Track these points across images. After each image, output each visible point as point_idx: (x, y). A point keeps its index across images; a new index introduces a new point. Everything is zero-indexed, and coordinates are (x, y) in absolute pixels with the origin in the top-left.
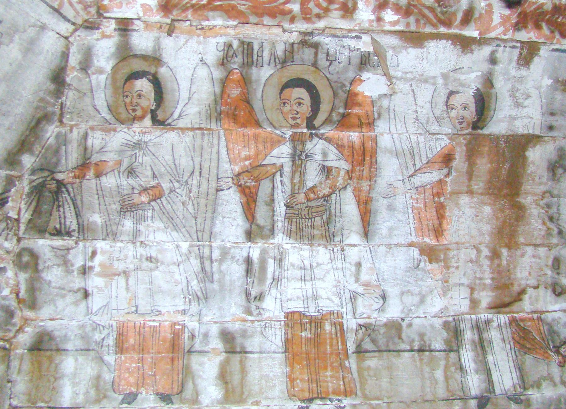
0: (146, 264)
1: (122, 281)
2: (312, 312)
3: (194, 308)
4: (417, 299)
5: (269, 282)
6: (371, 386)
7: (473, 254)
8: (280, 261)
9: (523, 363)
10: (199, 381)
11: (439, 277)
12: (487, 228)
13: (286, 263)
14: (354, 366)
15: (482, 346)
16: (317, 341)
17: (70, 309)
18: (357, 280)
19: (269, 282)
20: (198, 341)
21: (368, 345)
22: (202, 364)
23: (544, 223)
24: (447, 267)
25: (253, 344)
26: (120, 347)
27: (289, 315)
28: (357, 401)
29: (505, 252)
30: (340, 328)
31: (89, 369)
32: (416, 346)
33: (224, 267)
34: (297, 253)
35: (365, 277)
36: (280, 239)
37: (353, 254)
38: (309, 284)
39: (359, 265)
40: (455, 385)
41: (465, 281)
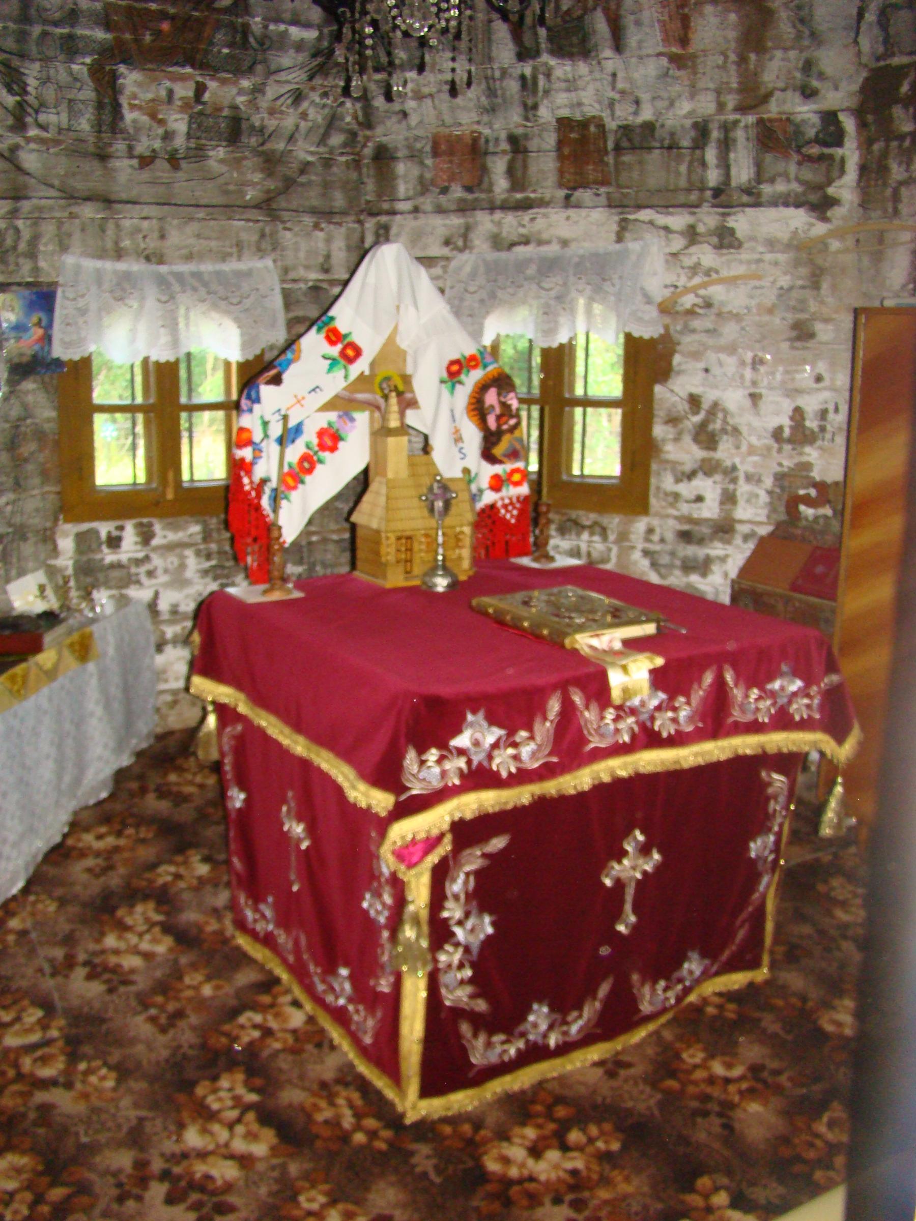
1: (429, 101)
2: (578, 117)
3: (485, 118)
4: (666, 103)
5: (540, 94)
6: (624, 177)
7: (720, 60)
8: (548, 75)
11: (687, 83)
12: (732, 35)
13: (553, 78)
15: (726, 145)
16: (584, 140)
18: (613, 88)
21: (625, 144)
23: (794, 27)
24: (695, 73)
25: (533, 145)
26: (435, 153)
27: (560, 121)
28: (610, 190)
29: (753, 57)
30: (601, 126)
31: (415, 171)
32: (666, 143)
33: (505, 83)
34: (562, 69)
35: (620, 85)
36: (545, 58)
37: (609, 66)
38: (573, 94)
39: (614, 75)
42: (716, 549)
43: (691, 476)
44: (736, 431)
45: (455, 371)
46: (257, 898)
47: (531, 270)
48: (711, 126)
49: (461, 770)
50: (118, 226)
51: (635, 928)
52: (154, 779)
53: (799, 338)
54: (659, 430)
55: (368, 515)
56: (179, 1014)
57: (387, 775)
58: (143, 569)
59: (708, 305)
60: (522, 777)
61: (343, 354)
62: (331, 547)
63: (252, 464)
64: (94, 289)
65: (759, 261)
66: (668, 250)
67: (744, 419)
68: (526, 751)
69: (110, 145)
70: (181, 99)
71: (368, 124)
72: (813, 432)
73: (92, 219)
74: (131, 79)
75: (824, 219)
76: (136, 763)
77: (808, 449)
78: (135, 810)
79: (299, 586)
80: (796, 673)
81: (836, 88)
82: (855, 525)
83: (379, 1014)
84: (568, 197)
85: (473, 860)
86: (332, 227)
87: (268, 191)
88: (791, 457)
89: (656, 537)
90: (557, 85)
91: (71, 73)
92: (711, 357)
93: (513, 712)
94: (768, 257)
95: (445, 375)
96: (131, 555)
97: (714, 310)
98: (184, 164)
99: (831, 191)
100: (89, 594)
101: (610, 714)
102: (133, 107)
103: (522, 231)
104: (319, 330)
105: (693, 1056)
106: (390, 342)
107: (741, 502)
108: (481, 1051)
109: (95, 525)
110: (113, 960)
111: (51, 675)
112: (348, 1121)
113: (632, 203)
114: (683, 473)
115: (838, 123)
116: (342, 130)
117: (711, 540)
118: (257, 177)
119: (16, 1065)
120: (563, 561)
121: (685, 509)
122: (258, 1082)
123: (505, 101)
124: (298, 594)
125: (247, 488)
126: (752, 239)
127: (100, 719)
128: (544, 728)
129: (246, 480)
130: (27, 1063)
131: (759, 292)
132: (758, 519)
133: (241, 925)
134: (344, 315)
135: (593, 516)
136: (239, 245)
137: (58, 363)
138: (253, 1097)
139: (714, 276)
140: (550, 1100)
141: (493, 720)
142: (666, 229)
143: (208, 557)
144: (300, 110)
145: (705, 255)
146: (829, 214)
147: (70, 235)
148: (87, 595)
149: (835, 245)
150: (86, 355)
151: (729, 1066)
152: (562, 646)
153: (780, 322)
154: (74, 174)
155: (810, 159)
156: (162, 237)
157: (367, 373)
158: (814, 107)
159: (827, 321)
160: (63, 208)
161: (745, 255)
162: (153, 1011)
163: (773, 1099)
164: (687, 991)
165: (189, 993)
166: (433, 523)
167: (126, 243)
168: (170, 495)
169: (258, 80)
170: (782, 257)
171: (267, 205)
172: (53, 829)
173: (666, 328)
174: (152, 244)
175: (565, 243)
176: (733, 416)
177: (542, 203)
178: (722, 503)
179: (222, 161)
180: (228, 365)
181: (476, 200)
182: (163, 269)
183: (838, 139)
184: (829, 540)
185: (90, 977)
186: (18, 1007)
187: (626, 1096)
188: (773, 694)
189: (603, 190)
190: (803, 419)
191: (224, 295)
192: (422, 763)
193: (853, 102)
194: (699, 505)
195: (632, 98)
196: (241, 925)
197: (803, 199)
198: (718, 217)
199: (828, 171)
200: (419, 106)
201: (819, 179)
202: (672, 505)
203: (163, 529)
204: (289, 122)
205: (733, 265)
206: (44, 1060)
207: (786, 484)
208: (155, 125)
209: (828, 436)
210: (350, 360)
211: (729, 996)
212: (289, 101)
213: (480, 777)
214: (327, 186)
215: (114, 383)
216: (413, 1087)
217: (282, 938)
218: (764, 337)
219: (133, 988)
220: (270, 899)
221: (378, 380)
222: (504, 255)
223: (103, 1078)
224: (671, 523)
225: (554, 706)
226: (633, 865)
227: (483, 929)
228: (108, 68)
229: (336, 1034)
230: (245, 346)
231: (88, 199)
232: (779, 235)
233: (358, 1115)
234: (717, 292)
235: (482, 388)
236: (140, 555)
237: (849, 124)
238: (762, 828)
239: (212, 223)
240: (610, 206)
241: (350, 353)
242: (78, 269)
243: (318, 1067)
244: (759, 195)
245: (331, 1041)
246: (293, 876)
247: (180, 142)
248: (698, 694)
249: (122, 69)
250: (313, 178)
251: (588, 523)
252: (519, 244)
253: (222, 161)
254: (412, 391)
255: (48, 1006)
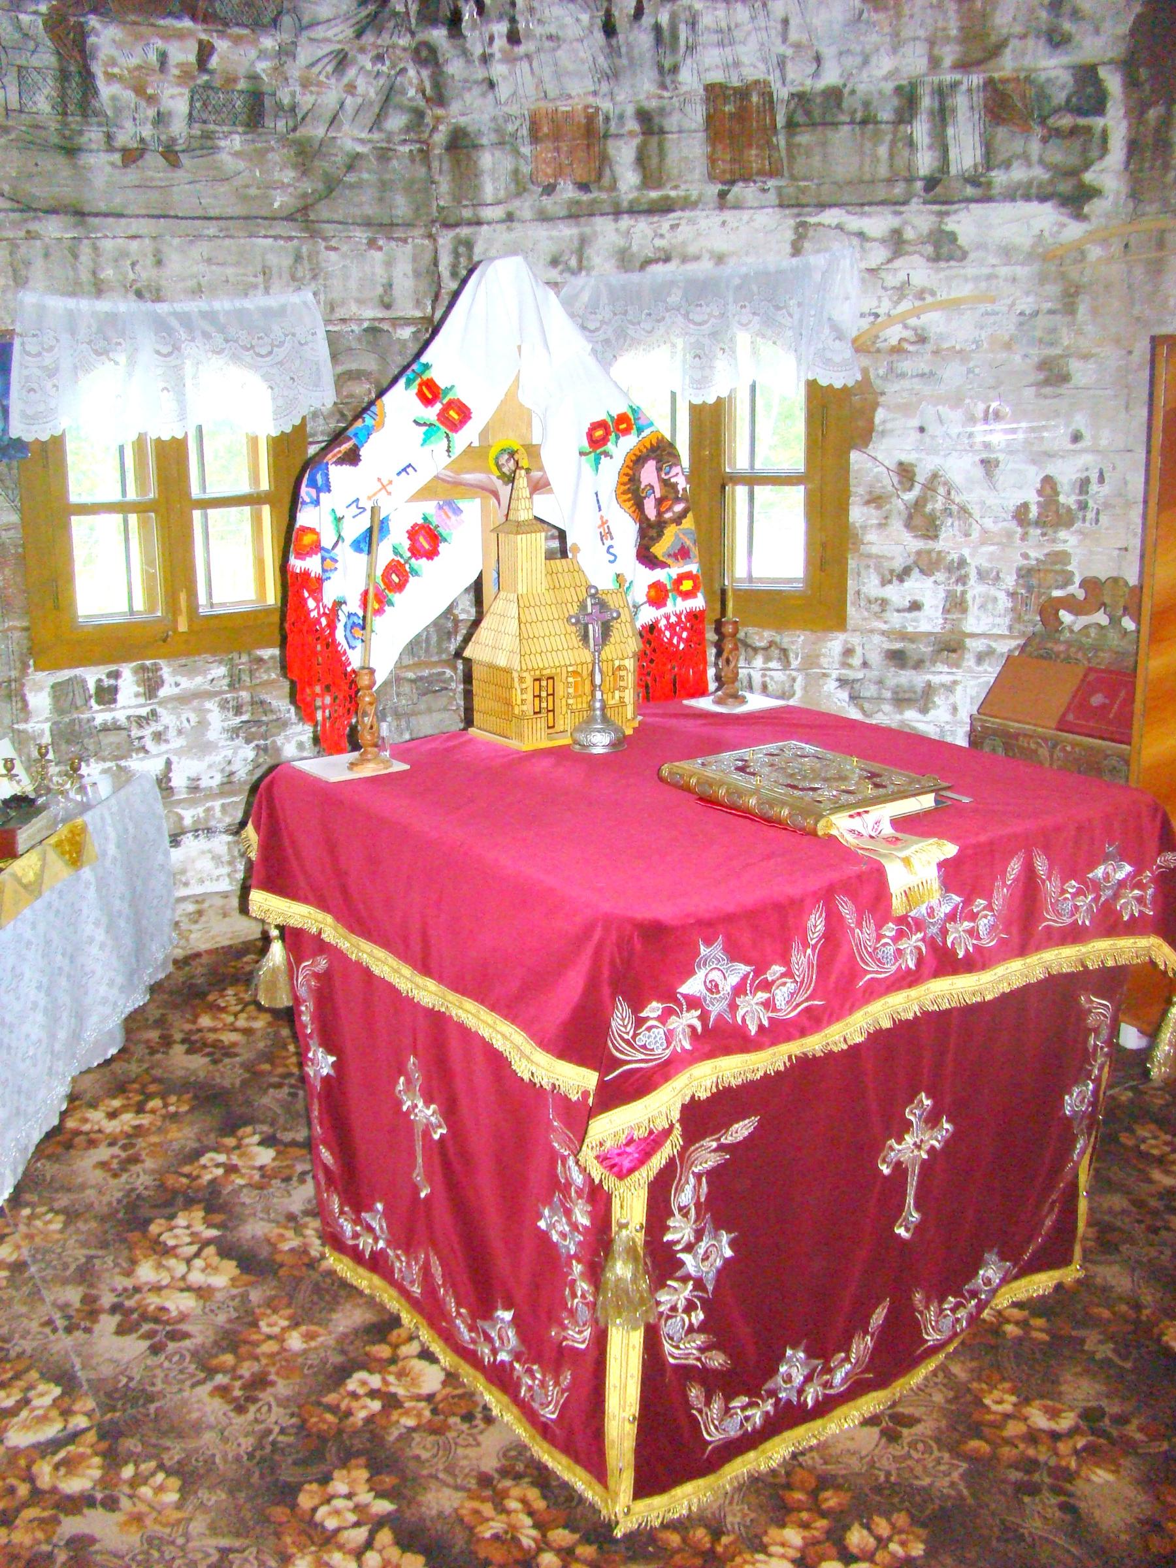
0: (548, 44)
2: (735, 83)
3: (605, 87)
4: (859, 60)
5: (682, 50)
8: (693, 25)
9: (993, 137)
10: (617, 168)
11: (887, 30)
13: (700, 26)
14: (782, 144)
15: (942, 116)
16: (741, 116)
17: (478, 103)
19: (682, 50)
20: (613, 123)
21: (800, 118)
22: (619, 149)
24: (899, 15)
25: (671, 123)
26: (535, 136)
27: (710, 88)
30: (768, 96)
31: (507, 163)
32: (859, 116)
35: (794, 36)
38: (728, 50)
39: (786, 22)
40: (900, 164)
41: (922, 33)
42: (940, 674)
43: (903, 575)
44: (963, 510)
45: (599, 436)
46: (358, 1204)
47: (675, 298)
48: (920, 90)
49: (693, 1028)
50: (95, 248)
51: (919, 1229)
52: (179, 1026)
53: (1047, 382)
54: (857, 514)
55: (493, 646)
56: (260, 1382)
57: (581, 1040)
58: (147, 732)
59: (922, 340)
60: (776, 1032)
61: (443, 417)
62: (406, 688)
63: (320, 581)
64: (65, 338)
65: (989, 277)
66: (863, 265)
67: (973, 494)
68: (781, 995)
69: (81, 133)
70: (178, 65)
71: (439, 99)
72: (1069, 510)
73: (60, 239)
74: (106, 37)
75: (1079, 216)
76: (151, 1000)
77: (1062, 534)
78: (158, 1072)
79: (400, 752)
80: (1123, 856)
81: (1097, 31)
82: (1155, 638)
83: (567, 1378)
84: (722, 195)
85: (707, 1156)
86: (393, 244)
87: (305, 195)
88: (1040, 545)
89: (856, 661)
90: (704, 38)
91: (19, 27)
92: (929, 412)
93: (759, 936)
94: (1003, 271)
95: (587, 448)
96: (130, 712)
97: (929, 347)
98: (185, 159)
99: (1088, 177)
100: (75, 769)
101: (890, 930)
102: (111, 77)
103: (659, 243)
104: (408, 384)
105: (999, 1401)
106: (511, 397)
107: (973, 609)
108: (718, 1421)
109: (78, 671)
110: (153, 1301)
111: (33, 889)
112: (528, 1536)
113: (814, 201)
114: (892, 571)
115: (1098, 83)
116: (401, 108)
117: (933, 662)
118: (288, 176)
119: (30, 1478)
120: (756, 702)
121: (895, 620)
122: (388, 1480)
123: (631, 60)
124: (400, 767)
125: (314, 614)
126: (981, 246)
127: (102, 946)
128: (803, 960)
129: (311, 604)
130: (44, 1471)
131: (992, 319)
132: (995, 631)
133: (334, 1240)
134: (444, 361)
135: (768, 635)
136: (266, 272)
137: (19, 445)
138: (384, 1506)
139: (929, 299)
140: (812, 1483)
141: (735, 953)
142: (861, 235)
143: (238, 711)
144: (346, 80)
145: (916, 270)
146: (1086, 209)
147: (28, 264)
148: (74, 770)
149: (1095, 252)
150: (58, 433)
151: (1054, 1414)
152: (814, 833)
153: (1022, 360)
154: (31, 176)
155: (1057, 133)
156: (159, 263)
157: (476, 444)
158: (1065, 60)
159: (1086, 357)
160: (15, 225)
161: (970, 271)
162: (220, 1379)
163: (1126, 1462)
164: (981, 1307)
165: (270, 1347)
166: (586, 655)
167: (108, 273)
168: (183, 627)
169: (285, 37)
170: (1022, 272)
171: (302, 216)
172: (46, 1106)
173: (865, 371)
174: (146, 273)
175: (720, 259)
176: (958, 491)
177: (688, 204)
178: (946, 611)
179: (236, 155)
180: (254, 442)
181: (594, 202)
182: (162, 308)
183: (1098, 106)
184: (1129, 662)
185: (121, 1331)
186: (22, 1383)
187: (918, 1470)
188: (1096, 886)
189: (771, 183)
190: (1057, 494)
191: (248, 341)
192: (640, 1022)
193: (1118, 51)
194: (915, 614)
195: (811, 54)
196: (334, 1240)
197: (1050, 189)
198: (933, 218)
199: (1085, 150)
200: (512, 73)
201: (1073, 160)
202: (877, 616)
203: (174, 673)
204: (331, 97)
205: (955, 283)
206: (70, 1465)
207: (1034, 582)
208: (143, 104)
209: (1090, 515)
210: (455, 427)
211: (1034, 1306)
212: (330, 69)
213: (721, 1038)
214: (384, 186)
215: (95, 471)
216: (624, 1483)
217: (399, 1262)
218: (999, 384)
219: (187, 1343)
220: (379, 1206)
221: (493, 453)
222: (635, 277)
223: (161, 1489)
224: (877, 639)
225: (816, 924)
226: (915, 1144)
227: (719, 1250)
228: (72, 20)
229: (492, 1398)
230: (278, 414)
231: (54, 211)
232: (1017, 241)
233: (541, 1525)
234: (933, 321)
235: (637, 461)
236: (143, 712)
237: (1113, 82)
238: (1081, 1075)
239: (227, 242)
240: (781, 206)
241: (456, 415)
242: (42, 309)
243: (471, 1452)
244: (989, 185)
245: (486, 1408)
246: (418, 1176)
247: (178, 128)
248: (1001, 895)
249: (93, 21)
250: (365, 176)
251: (763, 644)
252: (656, 261)
253: (236, 155)
254: (542, 469)
255: (66, 1379)
